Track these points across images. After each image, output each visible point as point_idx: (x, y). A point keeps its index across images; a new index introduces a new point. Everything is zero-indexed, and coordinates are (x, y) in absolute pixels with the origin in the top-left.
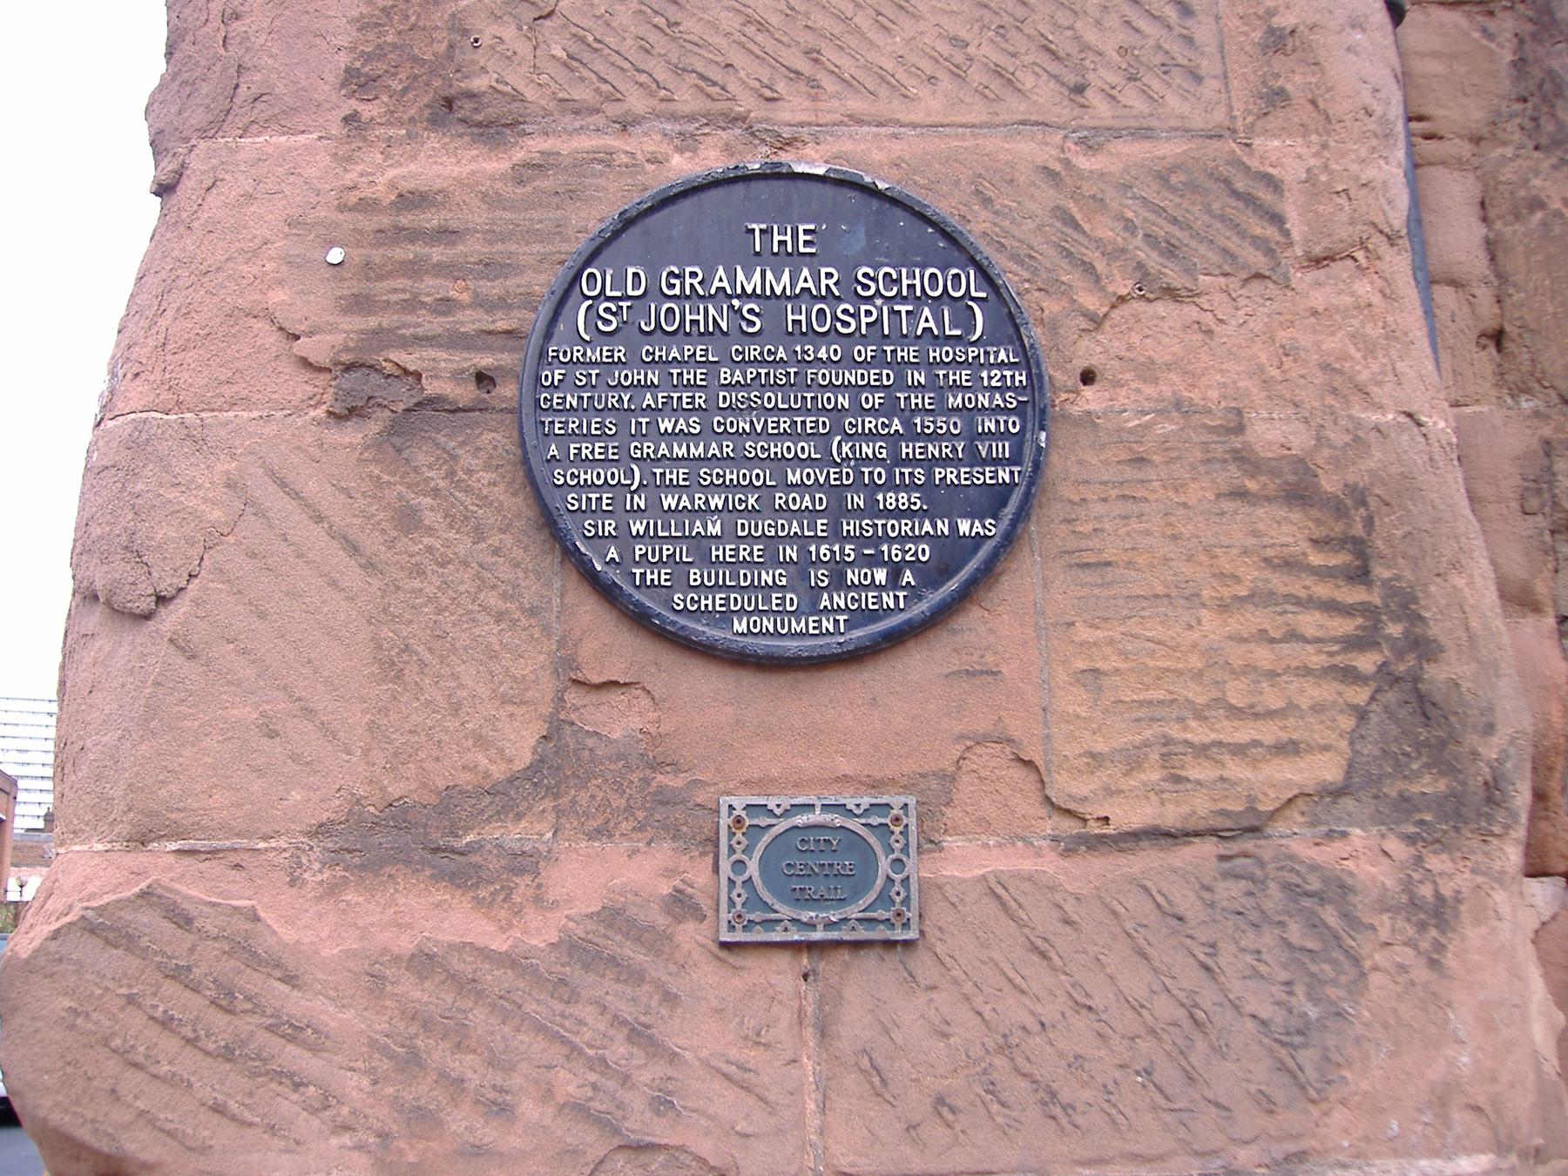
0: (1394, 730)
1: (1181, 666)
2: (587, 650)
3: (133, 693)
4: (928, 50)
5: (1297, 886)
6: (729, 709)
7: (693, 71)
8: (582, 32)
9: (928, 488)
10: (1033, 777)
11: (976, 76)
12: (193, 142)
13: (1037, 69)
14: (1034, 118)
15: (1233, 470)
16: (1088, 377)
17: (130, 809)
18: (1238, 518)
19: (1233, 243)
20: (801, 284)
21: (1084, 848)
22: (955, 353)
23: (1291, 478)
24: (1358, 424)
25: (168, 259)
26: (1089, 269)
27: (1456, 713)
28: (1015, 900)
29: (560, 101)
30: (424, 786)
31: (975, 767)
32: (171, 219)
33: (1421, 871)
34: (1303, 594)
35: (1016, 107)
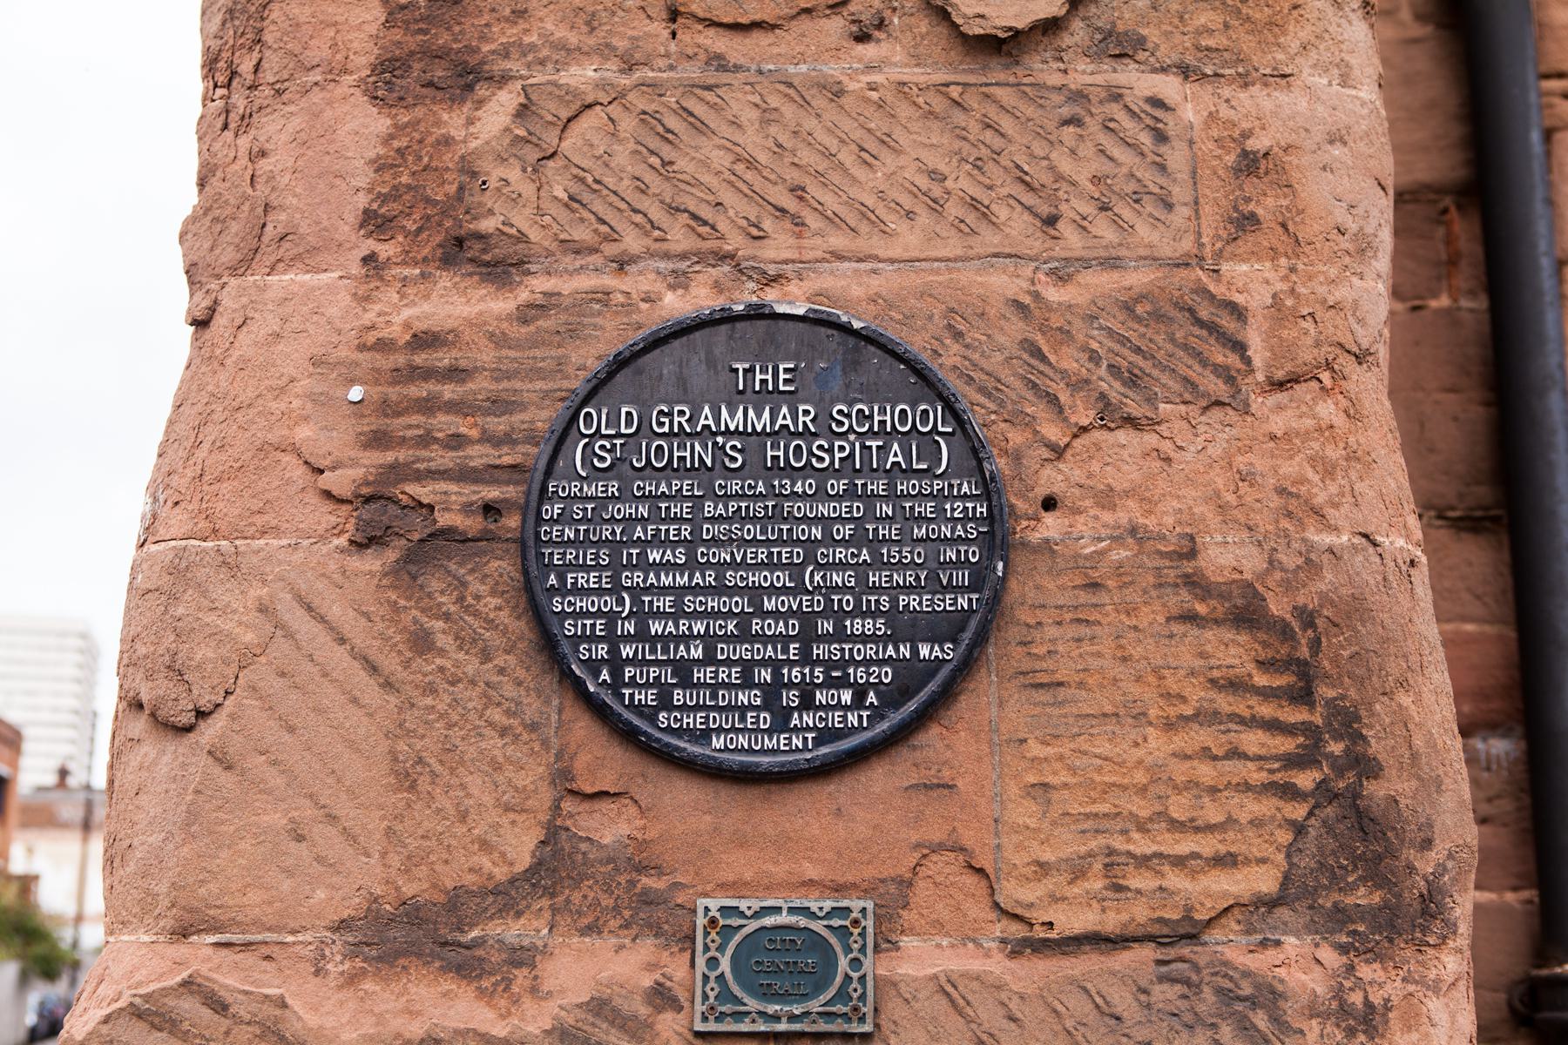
0: (1331, 843)
1: (1126, 781)
2: (581, 762)
3: (175, 800)
4: (907, 185)
5: (1230, 991)
6: (708, 818)
7: (685, 211)
8: (582, 174)
9: (892, 616)
10: (984, 883)
11: (953, 210)
12: (224, 279)
13: (1012, 202)
14: (1007, 250)
15: (1185, 594)
16: (1049, 504)
17: (173, 906)
18: (1187, 641)
19: (1195, 371)
20: (780, 422)
21: (1029, 951)
22: (921, 486)
23: (1240, 602)
24: (1311, 546)
25: (203, 393)
26: (1053, 400)
27: (1394, 829)
28: (964, 998)
29: (562, 241)
30: (434, 886)
31: (931, 873)
32: (206, 352)
33: (1353, 979)
34: (1246, 713)
35: (990, 240)
